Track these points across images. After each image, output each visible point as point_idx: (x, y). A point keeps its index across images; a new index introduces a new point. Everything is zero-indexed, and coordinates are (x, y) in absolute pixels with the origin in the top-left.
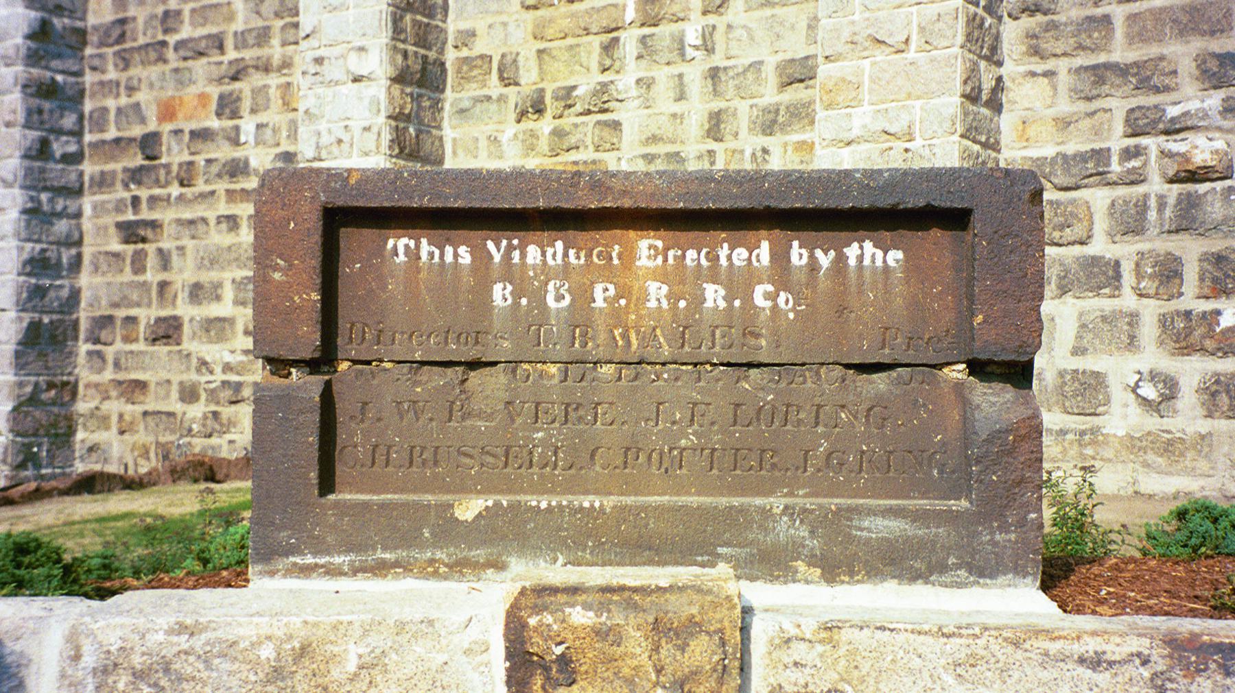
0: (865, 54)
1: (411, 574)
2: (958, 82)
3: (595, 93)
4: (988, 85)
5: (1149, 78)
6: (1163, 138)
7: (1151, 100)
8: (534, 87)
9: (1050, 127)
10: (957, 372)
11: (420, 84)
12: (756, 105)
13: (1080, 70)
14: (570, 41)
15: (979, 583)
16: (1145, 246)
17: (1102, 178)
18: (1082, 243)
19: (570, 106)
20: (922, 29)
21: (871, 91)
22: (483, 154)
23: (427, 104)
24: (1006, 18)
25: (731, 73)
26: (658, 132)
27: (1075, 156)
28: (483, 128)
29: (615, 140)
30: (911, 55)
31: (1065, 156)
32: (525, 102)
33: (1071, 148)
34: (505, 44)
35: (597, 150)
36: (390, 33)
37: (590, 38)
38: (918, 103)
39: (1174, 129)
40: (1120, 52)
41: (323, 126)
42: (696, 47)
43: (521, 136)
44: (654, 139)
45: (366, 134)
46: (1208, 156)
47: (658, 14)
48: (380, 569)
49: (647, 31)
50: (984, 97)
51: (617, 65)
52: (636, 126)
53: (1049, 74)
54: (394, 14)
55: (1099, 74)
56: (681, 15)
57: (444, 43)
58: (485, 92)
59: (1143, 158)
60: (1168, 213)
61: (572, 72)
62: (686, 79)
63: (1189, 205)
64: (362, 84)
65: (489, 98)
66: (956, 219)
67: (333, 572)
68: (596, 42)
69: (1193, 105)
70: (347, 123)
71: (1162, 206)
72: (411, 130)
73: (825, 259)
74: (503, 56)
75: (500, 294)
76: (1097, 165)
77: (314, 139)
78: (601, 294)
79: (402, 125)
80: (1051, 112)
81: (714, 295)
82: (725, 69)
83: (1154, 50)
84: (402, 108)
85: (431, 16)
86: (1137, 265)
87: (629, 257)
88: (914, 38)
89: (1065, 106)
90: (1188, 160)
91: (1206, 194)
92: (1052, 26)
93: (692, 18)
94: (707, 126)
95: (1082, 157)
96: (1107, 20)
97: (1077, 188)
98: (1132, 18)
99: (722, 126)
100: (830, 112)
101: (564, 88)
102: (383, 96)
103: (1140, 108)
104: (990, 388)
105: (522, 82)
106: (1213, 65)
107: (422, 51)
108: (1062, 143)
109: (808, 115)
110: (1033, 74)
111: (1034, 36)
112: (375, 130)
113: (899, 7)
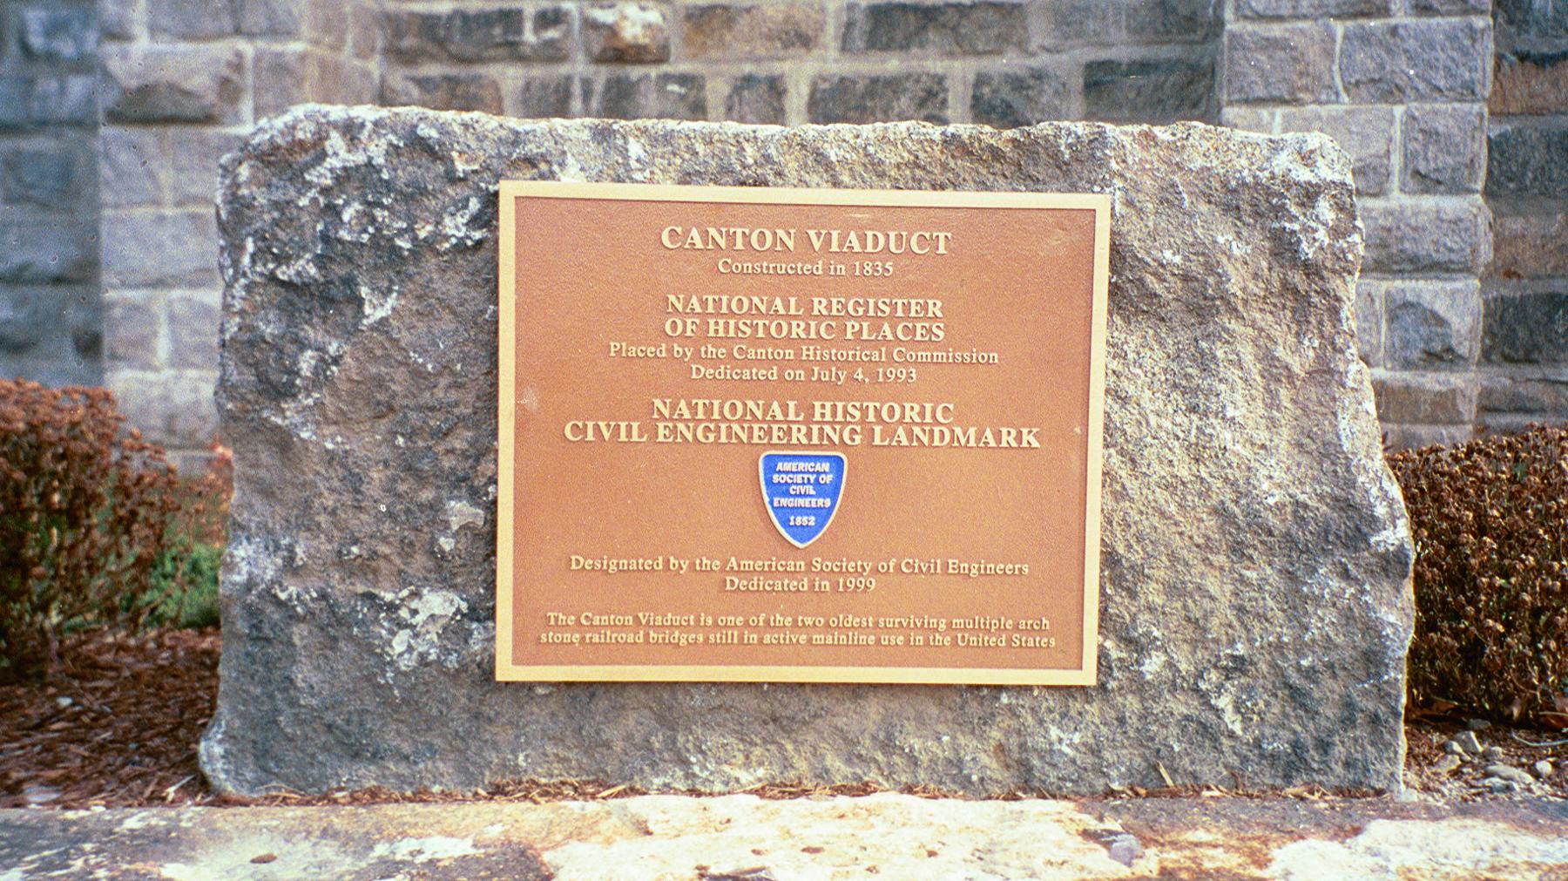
1: (1079, 35)
15: (1535, 822)
17: (514, 52)
46: (638, 30)
59: (563, 27)
76: (505, 33)
91: (640, 80)
104: (1258, 126)
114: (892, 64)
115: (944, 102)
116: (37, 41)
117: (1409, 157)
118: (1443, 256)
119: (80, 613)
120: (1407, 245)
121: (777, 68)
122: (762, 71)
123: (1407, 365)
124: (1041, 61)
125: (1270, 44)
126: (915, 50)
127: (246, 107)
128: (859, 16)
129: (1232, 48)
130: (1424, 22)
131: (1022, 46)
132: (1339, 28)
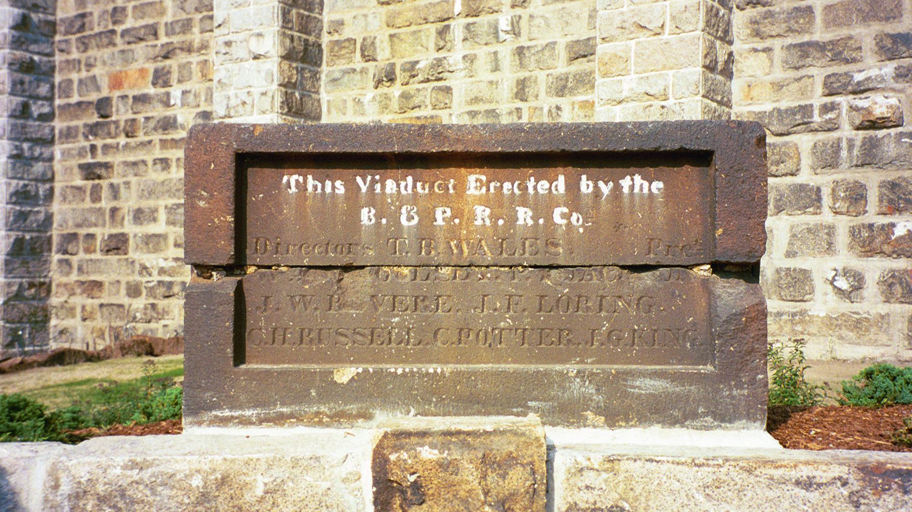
0: (631, 36)
3: (432, 67)
4: (722, 58)
5: (841, 53)
6: (852, 96)
8: (387, 62)
10: (704, 271)
11: (303, 60)
13: (790, 47)
14: (414, 28)
15: (721, 426)
16: (838, 177)
17: (807, 126)
18: (792, 175)
19: (414, 76)
20: (673, 18)
21: (636, 64)
22: (350, 111)
23: (308, 75)
24: (735, 9)
25: (533, 51)
27: (787, 110)
28: (350, 92)
29: (447, 101)
30: (666, 36)
31: (779, 110)
33: (784, 105)
34: (366, 30)
36: (280, 23)
37: (428, 26)
38: (671, 72)
39: (859, 91)
40: (820, 34)
41: (231, 92)
42: (507, 32)
43: (378, 99)
44: (476, 100)
45: (263, 98)
46: (884, 110)
48: (279, 420)
49: (470, 20)
51: (449, 45)
54: (283, 10)
56: (496, 8)
58: (351, 66)
60: (856, 152)
62: (499, 56)
64: (260, 60)
65: (354, 70)
66: (702, 158)
67: (245, 422)
68: (433, 28)
69: (873, 73)
71: (851, 146)
72: (297, 94)
73: (606, 189)
75: (367, 216)
76: (803, 117)
78: (441, 215)
79: (289, 91)
81: (524, 215)
83: (844, 32)
84: (290, 78)
85: (310, 10)
86: (833, 190)
87: (461, 187)
89: (779, 74)
90: (870, 113)
94: (515, 90)
95: (792, 112)
97: (789, 134)
99: (527, 90)
102: (276, 70)
103: (834, 75)
105: (379, 58)
106: (888, 43)
107: (304, 36)
110: (755, 50)
111: (756, 22)
112: (270, 94)
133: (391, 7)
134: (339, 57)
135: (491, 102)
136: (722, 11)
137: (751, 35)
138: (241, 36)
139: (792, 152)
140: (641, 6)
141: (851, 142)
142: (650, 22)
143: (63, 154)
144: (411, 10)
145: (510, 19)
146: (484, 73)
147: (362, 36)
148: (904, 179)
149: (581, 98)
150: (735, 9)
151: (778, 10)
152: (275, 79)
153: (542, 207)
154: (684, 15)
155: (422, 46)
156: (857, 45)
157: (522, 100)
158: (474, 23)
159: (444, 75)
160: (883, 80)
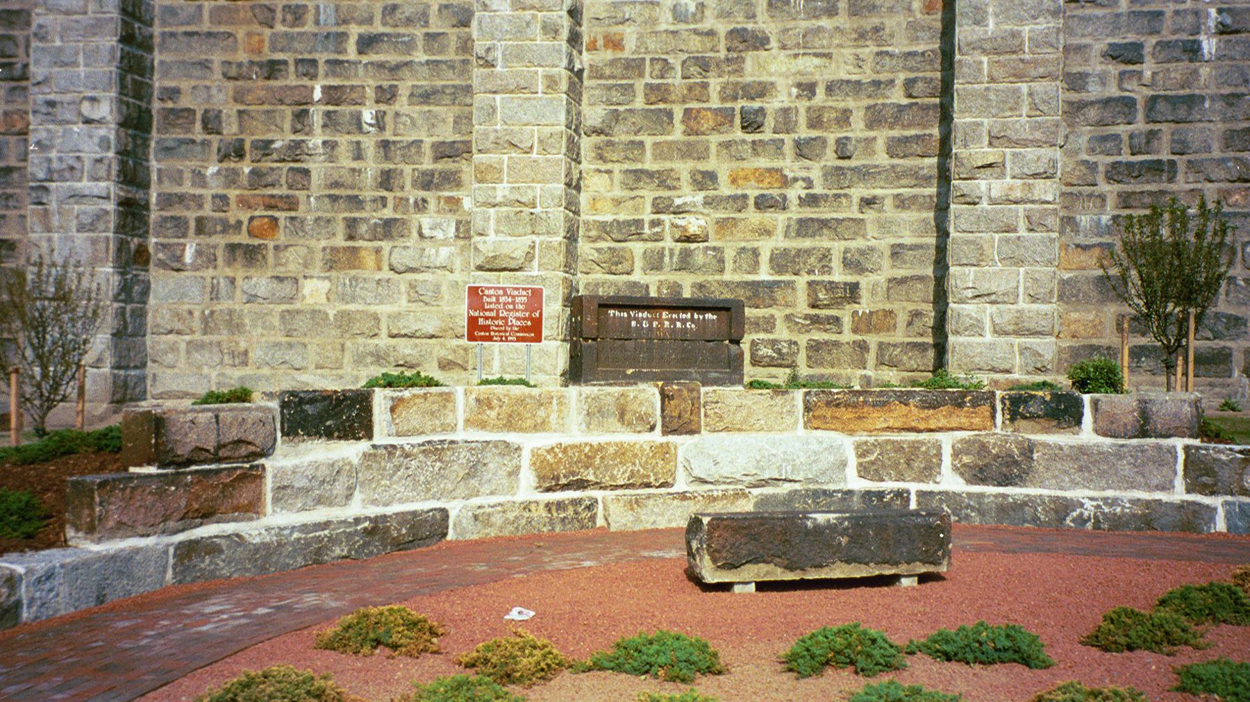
0: (505, 151)
2: (563, 175)
3: (289, 148)
4: (575, 176)
5: (665, 181)
6: (672, 216)
7: (667, 193)
8: (234, 137)
9: (609, 204)
10: (727, 342)
11: (136, 128)
12: (417, 169)
13: (627, 171)
14: (266, 107)
16: (662, 277)
17: (639, 236)
18: (628, 274)
19: (268, 155)
20: (541, 141)
21: (509, 174)
22: (188, 183)
23: (139, 142)
24: (583, 135)
25: (398, 146)
26: (339, 180)
27: (624, 222)
28: (188, 163)
29: (306, 183)
30: (534, 155)
31: (618, 222)
32: (228, 148)
33: (622, 217)
34: (208, 102)
35: (290, 187)
36: (118, 90)
37: (283, 107)
38: (539, 186)
39: (678, 211)
40: (649, 164)
41: (53, 154)
42: (371, 125)
43: (224, 173)
44: (336, 184)
45: (98, 166)
47: (339, 98)
48: (611, 385)
49: (331, 108)
50: (574, 184)
51: (307, 129)
52: (322, 173)
53: (609, 172)
54: (121, 74)
55: (638, 175)
56: (359, 101)
57: (152, 94)
58: (189, 136)
60: (675, 259)
61: (269, 130)
62: (363, 146)
63: (686, 256)
64: (93, 126)
65: (193, 142)
66: (727, 309)
67: (600, 385)
68: (288, 111)
69: (688, 199)
70: (78, 154)
71: (672, 255)
72: (130, 162)
73: (701, 317)
74: (206, 111)
75: (633, 323)
76: (637, 229)
77: (46, 165)
78: (655, 324)
79: (125, 158)
80: (610, 194)
81: (679, 325)
82: (394, 142)
83: (668, 165)
84: (126, 145)
85: (142, 75)
86: (659, 288)
87: (661, 315)
88: (536, 145)
89: (618, 192)
90: (686, 230)
92: (610, 144)
93: (367, 103)
94: (379, 180)
95: (628, 224)
96: (641, 144)
97: (625, 241)
98: (656, 144)
99: (392, 181)
100: (481, 185)
101: (262, 141)
102: (112, 137)
103: (660, 197)
105: (225, 132)
106: (699, 177)
107: (138, 102)
108: (616, 214)
109: (455, 180)
110: (600, 171)
111: (599, 148)
112: (106, 162)
113: (526, 125)
114: (807, 243)
115: (830, 260)
116: (426, 232)
117: (1026, 288)
118: (1040, 329)
119: (1172, 225)
120: (1025, 324)
121: (756, 244)
122: (749, 245)
123: (1029, 373)
124: (873, 243)
125: (968, 242)
126: (817, 238)
127: (535, 263)
128: (793, 223)
129: (953, 243)
130: (1031, 234)
131: (864, 236)
132: (997, 236)
133: (239, 83)
134: (174, 126)
135: (353, 188)
136: (576, 138)
137: (595, 158)
138: (67, 97)
139: (627, 255)
140: (512, 127)
141: (671, 250)
142: (521, 142)
143: (199, 253)
144: (262, 89)
145: (374, 112)
146: (346, 161)
147: (203, 107)
148: (708, 282)
149: (447, 194)
150: (583, 135)
151: (617, 140)
152: (112, 146)
153: (684, 322)
154: (550, 141)
155: (276, 126)
156: (677, 176)
157: (387, 189)
158: (335, 112)
159: (302, 157)
160: (695, 206)
